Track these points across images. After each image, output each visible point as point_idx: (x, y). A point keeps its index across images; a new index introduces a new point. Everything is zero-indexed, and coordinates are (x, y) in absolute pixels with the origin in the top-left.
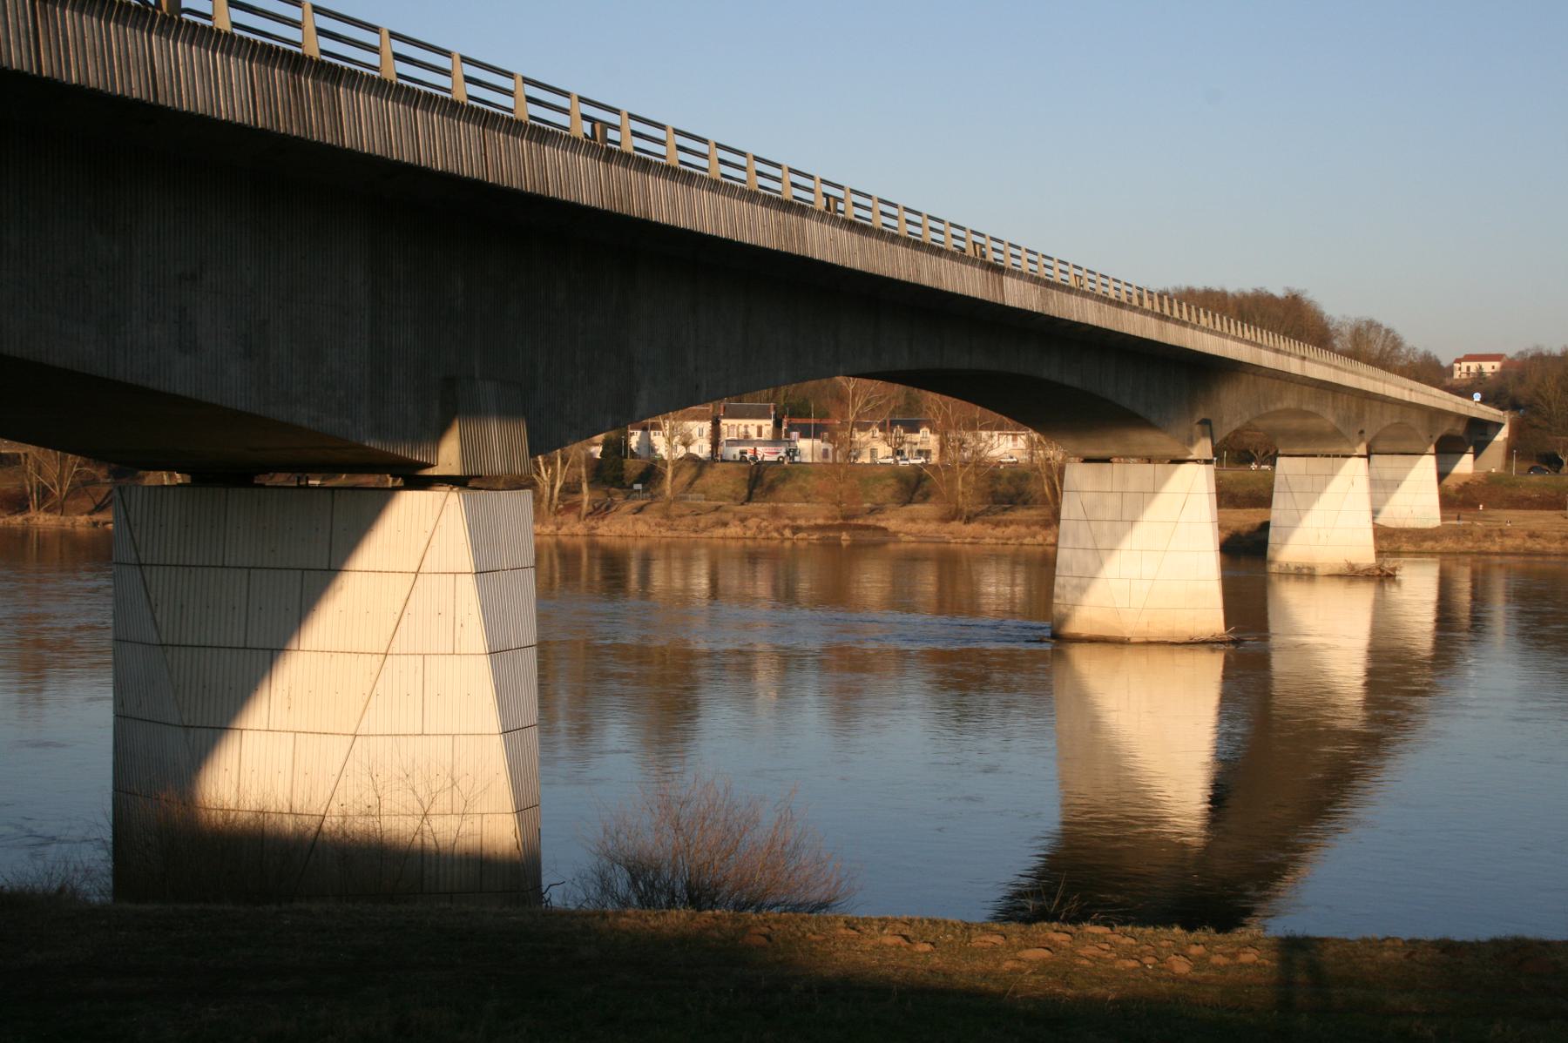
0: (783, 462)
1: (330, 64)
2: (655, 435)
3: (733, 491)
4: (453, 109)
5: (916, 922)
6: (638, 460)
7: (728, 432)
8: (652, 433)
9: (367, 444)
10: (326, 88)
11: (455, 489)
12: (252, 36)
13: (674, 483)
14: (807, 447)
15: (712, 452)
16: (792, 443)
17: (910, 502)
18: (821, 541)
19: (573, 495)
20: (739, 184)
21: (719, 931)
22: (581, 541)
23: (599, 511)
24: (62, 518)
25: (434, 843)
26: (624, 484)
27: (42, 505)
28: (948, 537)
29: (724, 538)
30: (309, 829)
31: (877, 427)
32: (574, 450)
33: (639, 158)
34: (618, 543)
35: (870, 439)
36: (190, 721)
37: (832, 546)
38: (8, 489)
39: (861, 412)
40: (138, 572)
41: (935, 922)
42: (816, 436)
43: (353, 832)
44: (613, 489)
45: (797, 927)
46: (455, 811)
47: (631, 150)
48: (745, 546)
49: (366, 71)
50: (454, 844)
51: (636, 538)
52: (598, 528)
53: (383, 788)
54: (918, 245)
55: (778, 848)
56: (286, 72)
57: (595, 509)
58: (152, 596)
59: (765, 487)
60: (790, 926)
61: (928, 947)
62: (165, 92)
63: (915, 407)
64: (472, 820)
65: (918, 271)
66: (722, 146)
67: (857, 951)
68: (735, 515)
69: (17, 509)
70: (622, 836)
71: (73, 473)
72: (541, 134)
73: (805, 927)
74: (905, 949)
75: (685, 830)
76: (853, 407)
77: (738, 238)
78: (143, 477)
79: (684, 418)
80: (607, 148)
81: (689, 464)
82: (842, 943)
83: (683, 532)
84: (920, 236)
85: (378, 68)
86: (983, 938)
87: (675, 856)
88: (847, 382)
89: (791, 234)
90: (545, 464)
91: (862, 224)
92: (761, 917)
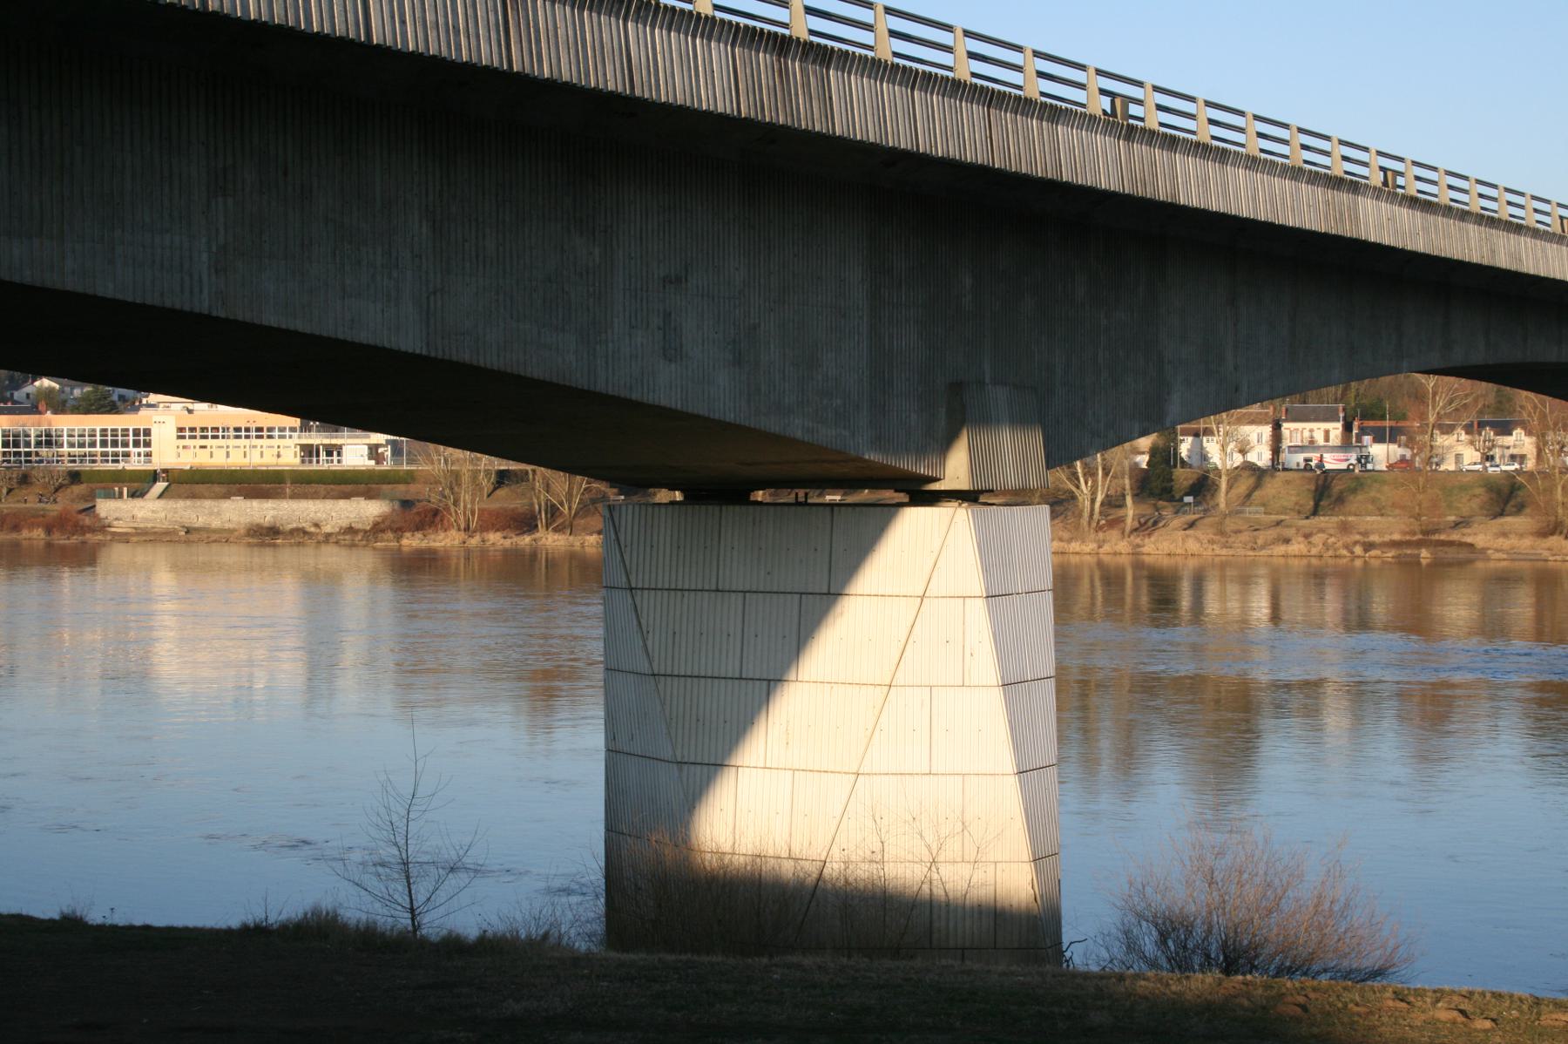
0: (1353, 470)
1: (819, 45)
2: (1208, 441)
3: (1296, 504)
4: (955, 88)
5: (1476, 996)
6: (1189, 470)
7: (1291, 437)
8: (1205, 439)
9: (867, 457)
10: (815, 72)
11: (963, 505)
12: (735, 19)
13: (1229, 496)
14: (1381, 454)
15: (1273, 460)
16: (1364, 449)
17: (1502, 514)
18: (1397, 560)
19: (1117, 509)
20: (1280, 160)
21: (1249, 999)
22: (1125, 560)
23: (1146, 527)
24: (571, 538)
25: (944, 894)
26: (1173, 496)
27: (551, 524)
28: (1546, 554)
29: (1285, 556)
30: (809, 876)
31: (1462, 429)
32: (1116, 459)
33: (1165, 135)
34: (1166, 562)
35: (1455, 443)
36: (683, 757)
37: (1412, 564)
38: (517, 508)
39: (1442, 412)
40: (629, 596)
41: (1500, 995)
42: (1393, 440)
43: (856, 880)
44: (1161, 502)
45: (1338, 996)
46: (967, 858)
47: (1156, 127)
48: (1309, 565)
49: (859, 51)
50: (965, 895)
51: (1186, 556)
52: (1144, 546)
53: (888, 832)
54: (1493, 222)
55: (1326, 906)
56: (771, 56)
57: (1141, 525)
58: (643, 622)
59: (1333, 499)
60: (1329, 995)
61: (1488, 1024)
62: (642, 83)
63: (1507, 406)
64: (984, 869)
65: (1493, 252)
66: (1450, 172)
67: (1405, 1026)
68: (1298, 530)
69: (525, 529)
70: (1149, 890)
71: (582, 490)
72: (1053, 112)
73: (1346, 996)
74: (1462, 1026)
75: (1220, 884)
76: (1434, 408)
77: (1281, 221)
78: (655, 494)
79: (1240, 421)
80: (1128, 125)
81: (1247, 473)
82: (1389, 1017)
83: (1239, 550)
84: (1495, 212)
85: (873, 47)
86: (1554, 1016)
87: (1210, 913)
88: (1426, 380)
89: (1341, 214)
90: (1085, 475)
91: (1425, 201)
92: (1297, 985)
